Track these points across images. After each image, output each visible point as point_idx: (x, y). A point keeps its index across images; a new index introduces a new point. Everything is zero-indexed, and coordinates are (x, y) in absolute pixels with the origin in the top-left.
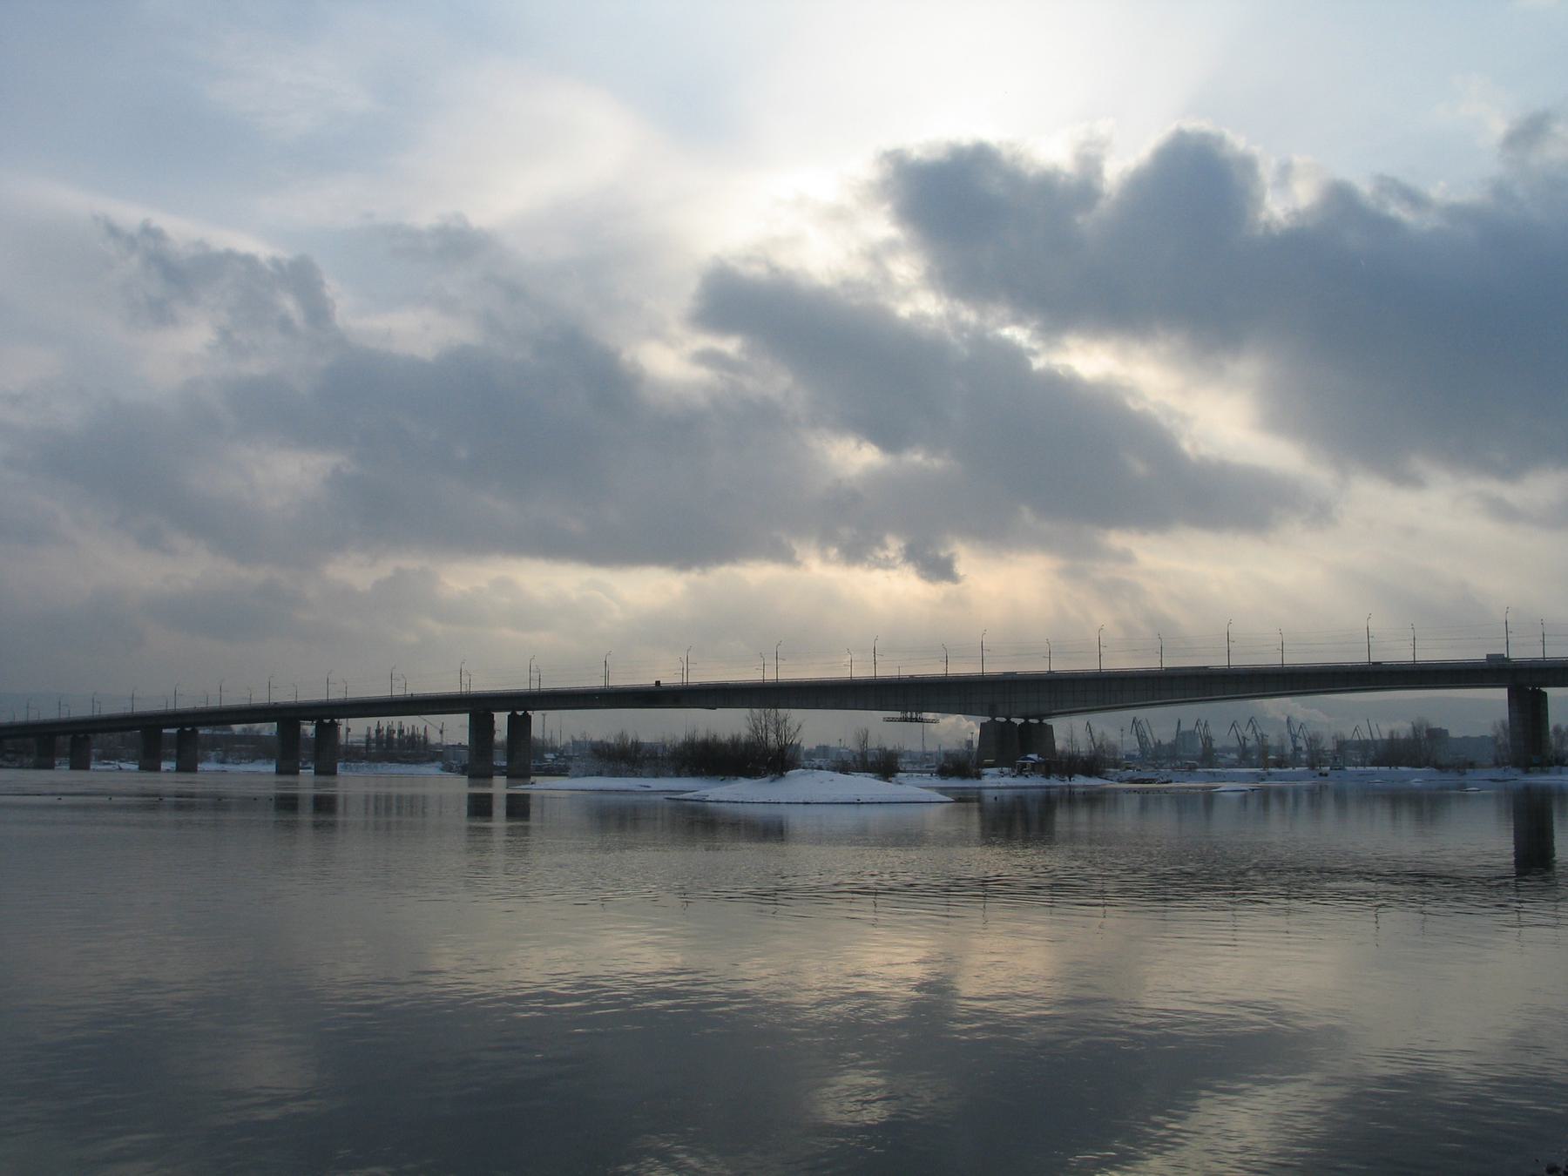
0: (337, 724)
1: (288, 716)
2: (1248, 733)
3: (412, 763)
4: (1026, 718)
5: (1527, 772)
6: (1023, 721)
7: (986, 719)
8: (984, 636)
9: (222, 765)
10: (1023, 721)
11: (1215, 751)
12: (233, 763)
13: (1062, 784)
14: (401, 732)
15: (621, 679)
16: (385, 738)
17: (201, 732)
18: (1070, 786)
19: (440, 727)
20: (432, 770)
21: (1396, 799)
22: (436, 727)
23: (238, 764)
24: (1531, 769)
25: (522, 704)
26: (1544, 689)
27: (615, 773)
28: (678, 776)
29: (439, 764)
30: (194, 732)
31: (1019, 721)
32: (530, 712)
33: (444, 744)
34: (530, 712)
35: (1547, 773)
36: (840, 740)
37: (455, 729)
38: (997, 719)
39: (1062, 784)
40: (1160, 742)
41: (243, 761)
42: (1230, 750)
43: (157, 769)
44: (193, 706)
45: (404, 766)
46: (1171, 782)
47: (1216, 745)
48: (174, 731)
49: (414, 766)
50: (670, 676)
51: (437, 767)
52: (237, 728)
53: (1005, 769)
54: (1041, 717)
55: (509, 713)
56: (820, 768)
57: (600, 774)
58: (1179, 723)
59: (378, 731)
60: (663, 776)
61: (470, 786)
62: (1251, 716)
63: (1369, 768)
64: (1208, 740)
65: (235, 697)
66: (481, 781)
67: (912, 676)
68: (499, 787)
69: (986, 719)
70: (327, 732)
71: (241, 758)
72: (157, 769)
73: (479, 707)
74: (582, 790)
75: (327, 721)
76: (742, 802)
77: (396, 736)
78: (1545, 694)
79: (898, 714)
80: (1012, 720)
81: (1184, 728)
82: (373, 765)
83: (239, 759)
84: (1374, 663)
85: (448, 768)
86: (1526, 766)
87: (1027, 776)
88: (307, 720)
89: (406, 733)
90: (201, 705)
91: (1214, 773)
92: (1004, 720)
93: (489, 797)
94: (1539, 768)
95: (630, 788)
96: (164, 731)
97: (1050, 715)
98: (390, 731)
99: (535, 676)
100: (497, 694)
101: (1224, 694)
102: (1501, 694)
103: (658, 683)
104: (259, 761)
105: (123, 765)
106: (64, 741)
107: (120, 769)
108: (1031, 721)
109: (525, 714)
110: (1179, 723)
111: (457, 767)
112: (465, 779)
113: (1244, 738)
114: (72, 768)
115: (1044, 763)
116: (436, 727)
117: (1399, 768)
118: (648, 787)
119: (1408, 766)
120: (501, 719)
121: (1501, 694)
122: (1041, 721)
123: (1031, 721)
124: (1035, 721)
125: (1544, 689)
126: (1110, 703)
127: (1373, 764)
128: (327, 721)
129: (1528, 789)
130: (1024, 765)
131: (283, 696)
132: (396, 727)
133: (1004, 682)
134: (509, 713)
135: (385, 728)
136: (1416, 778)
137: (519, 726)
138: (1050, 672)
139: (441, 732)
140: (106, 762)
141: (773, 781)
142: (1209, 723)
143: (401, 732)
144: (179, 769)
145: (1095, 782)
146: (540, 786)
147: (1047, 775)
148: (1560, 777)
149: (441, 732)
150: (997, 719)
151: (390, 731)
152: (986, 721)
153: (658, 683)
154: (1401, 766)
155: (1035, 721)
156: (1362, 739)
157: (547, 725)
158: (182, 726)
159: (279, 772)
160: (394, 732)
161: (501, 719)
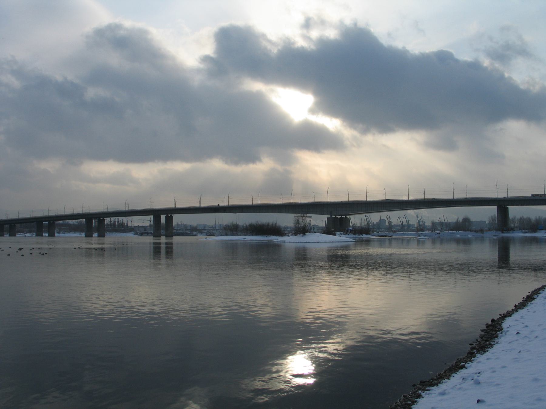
0: (105, 220)
1: (88, 217)
2: (404, 220)
3: (124, 232)
4: (341, 216)
5: (503, 232)
6: (340, 217)
7: (329, 216)
8: (328, 189)
9: (59, 234)
10: (340, 217)
11: (393, 226)
12: (63, 233)
13: (360, 237)
14: (118, 221)
15: (131, 208)
16: (113, 224)
17: (56, 223)
18: (362, 237)
19: (131, 220)
20: (131, 234)
21: (458, 241)
22: (130, 220)
23: (64, 234)
24: (504, 232)
25: (170, 212)
26: (507, 206)
27: (233, 235)
28: (253, 235)
29: (133, 232)
30: (54, 223)
31: (339, 217)
32: (172, 215)
33: (133, 226)
34: (172, 215)
35: (509, 233)
36: (362, 219)
37: (146, 221)
38: (332, 216)
39: (360, 237)
40: (374, 223)
41: (66, 233)
42: (397, 226)
43: (42, 236)
44: (55, 214)
45: (121, 233)
46: (392, 236)
47: (393, 224)
48: (47, 223)
49: (125, 233)
50: (194, 204)
51: (133, 233)
52: (61, 222)
53: (342, 232)
54: (346, 215)
55: (166, 215)
56: (315, 232)
57: (227, 235)
58: (381, 217)
59: (111, 221)
60: (248, 235)
61: (166, 239)
62: (404, 214)
63: (450, 232)
64: (390, 222)
65: (69, 211)
66: (169, 238)
67: (341, 201)
68: (163, 240)
69: (329, 216)
70: (101, 222)
71: (65, 231)
72: (42, 236)
73: (156, 213)
74: (216, 240)
75: (102, 219)
76: (298, 242)
77: (116, 224)
78: (508, 208)
79: (300, 215)
80: (337, 216)
81: (382, 218)
82: (111, 233)
83: (65, 232)
84: (387, 200)
85: (136, 234)
86: (503, 231)
87: (349, 235)
88: (60, 220)
89: (120, 222)
90: (29, 216)
91: (404, 234)
92: (334, 216)
93: (160, 243)
94: (506, 231)
95: (240, 239)
96: (44, 223)
97: (348, 215)
98: (115, 222)
99: (127, 206)
100: (236, 206)
101: (433, 206)
102: (495, 207)
103: (219, 205)
104: (71, 233)
105: (26, 235)
106: (7, 226)
107: (25, 236)
108: (343, 217)
109: (171, 216)
110: (381, 217)
111: (139, 233)
112: (152, 237)
113: (402, 222)
114: (10, 236)
115: (354, 230)
116: (130, 220)
117: (459, 232)
118: (246, 239)
119: (462, 231)
120: (163, 218)
121: (495, 207)
122: (346, 217)
123: (343, 217)
124: (344, 217)
125: (507, 206)
126: (372, 211)
127: (451, 230)
128: (102, 219)
129: (503, 238)
130: (348, 231)
131: (86, 210)
132: (117, 220)
133: (354, 203)
134: (166, 215)
135: (113, 221)
136: (460, 234)
137: (169, 220)
138: (82, 213)
139: (131, 221)
140: (19, 233)
141: (303, 236)
142: (390, 217)
143: (118, 221)
144: (49, 236)
145: (368, 236)
146: (176, 239)
147: (355, 234)
148: (513, 234)
149: (131, 221)
150: (332, 216)
151: (115, 222)
152: (329, 217)
153: (219, 205)
154: (460, 231)
155: (344, 217)
156: (441, 222)
157: (178, 219)
158: (49, 221)
159: (86, 236)
160: (116, 222)
161: (163, 218)
